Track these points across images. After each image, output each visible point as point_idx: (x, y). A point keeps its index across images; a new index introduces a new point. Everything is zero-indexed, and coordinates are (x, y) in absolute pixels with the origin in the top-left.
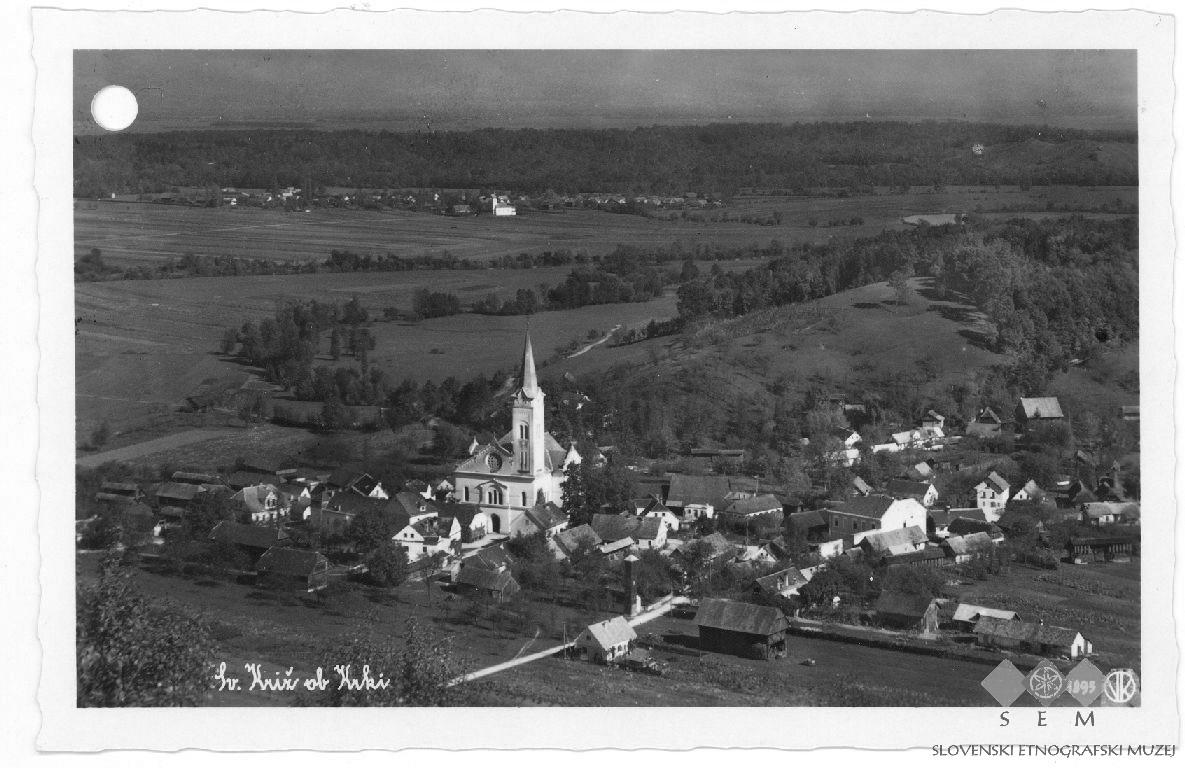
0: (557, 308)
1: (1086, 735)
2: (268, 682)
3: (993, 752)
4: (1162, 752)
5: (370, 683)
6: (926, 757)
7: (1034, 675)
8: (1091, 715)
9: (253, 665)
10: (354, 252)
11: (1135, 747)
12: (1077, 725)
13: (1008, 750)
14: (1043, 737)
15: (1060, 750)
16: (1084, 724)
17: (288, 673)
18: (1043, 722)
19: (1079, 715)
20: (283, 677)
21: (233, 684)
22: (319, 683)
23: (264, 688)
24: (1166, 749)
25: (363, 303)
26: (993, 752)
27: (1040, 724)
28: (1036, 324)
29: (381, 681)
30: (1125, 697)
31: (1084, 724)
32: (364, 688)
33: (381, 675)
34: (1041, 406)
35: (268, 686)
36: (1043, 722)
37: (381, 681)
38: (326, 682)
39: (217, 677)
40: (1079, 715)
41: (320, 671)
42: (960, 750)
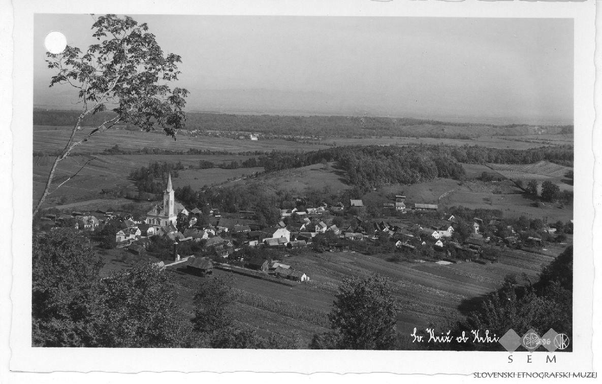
0: (245, 167)
1: (551, 368)
2: (438, 338)
3: (504, 376)
4: (587, 374)
5: (489, 339)
6: (471, 379)
7: (525, 337)
8: (554, 357)
9: (430, 329)
10: (196, 148)
11: (577, 374)
12: (547, 362)
13: (512, 375)
14: (530, 369)
15: (538, 375)
16: (551, 361)
17: (448, 334)
18: (530, 361)
19: (548, 357)
20: (445, 335)
21: (420, 339)
22: (463, 338)
23: (435, 341)
24: (591, 375)
25: (182, 163)
26: (504, 376)
27: (528, 362)
28: (363, 177)
29: (495, 339)
30: (564, 347)
31: (551, 361)
32: (446, 342)
33: (495, 335)
34: (357, 203)
35: (438, 340)
36: (530, 361)
37: (495, 339)
38: (467, 339)
39: (412, 335)
40: (548, 357)
41: (464, 333)
42: (488, 375)
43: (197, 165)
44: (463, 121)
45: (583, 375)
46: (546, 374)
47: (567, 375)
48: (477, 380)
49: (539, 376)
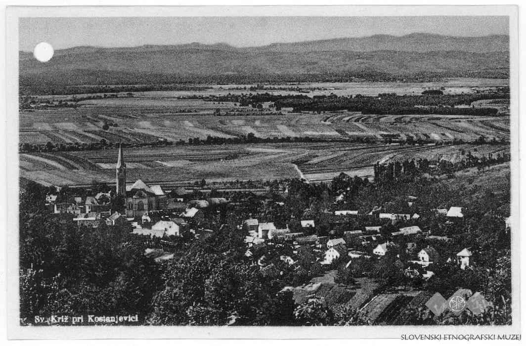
4: (511, 337)
43: (187, 141)
44: (350, 13)
45: (508, 337)
46: (472, 336)
47: (492, 337)
48: (405, 342)
49: (465, 338)
